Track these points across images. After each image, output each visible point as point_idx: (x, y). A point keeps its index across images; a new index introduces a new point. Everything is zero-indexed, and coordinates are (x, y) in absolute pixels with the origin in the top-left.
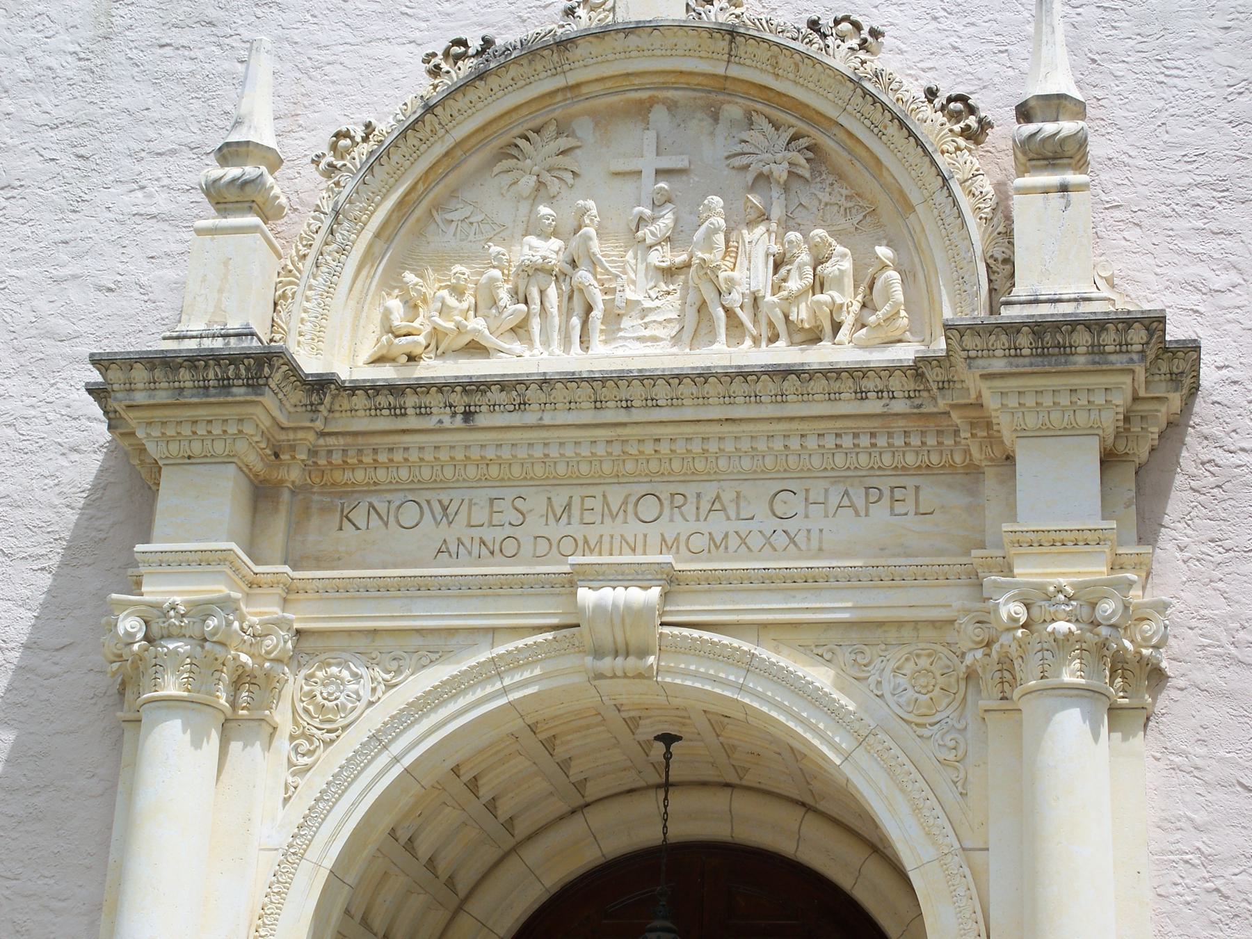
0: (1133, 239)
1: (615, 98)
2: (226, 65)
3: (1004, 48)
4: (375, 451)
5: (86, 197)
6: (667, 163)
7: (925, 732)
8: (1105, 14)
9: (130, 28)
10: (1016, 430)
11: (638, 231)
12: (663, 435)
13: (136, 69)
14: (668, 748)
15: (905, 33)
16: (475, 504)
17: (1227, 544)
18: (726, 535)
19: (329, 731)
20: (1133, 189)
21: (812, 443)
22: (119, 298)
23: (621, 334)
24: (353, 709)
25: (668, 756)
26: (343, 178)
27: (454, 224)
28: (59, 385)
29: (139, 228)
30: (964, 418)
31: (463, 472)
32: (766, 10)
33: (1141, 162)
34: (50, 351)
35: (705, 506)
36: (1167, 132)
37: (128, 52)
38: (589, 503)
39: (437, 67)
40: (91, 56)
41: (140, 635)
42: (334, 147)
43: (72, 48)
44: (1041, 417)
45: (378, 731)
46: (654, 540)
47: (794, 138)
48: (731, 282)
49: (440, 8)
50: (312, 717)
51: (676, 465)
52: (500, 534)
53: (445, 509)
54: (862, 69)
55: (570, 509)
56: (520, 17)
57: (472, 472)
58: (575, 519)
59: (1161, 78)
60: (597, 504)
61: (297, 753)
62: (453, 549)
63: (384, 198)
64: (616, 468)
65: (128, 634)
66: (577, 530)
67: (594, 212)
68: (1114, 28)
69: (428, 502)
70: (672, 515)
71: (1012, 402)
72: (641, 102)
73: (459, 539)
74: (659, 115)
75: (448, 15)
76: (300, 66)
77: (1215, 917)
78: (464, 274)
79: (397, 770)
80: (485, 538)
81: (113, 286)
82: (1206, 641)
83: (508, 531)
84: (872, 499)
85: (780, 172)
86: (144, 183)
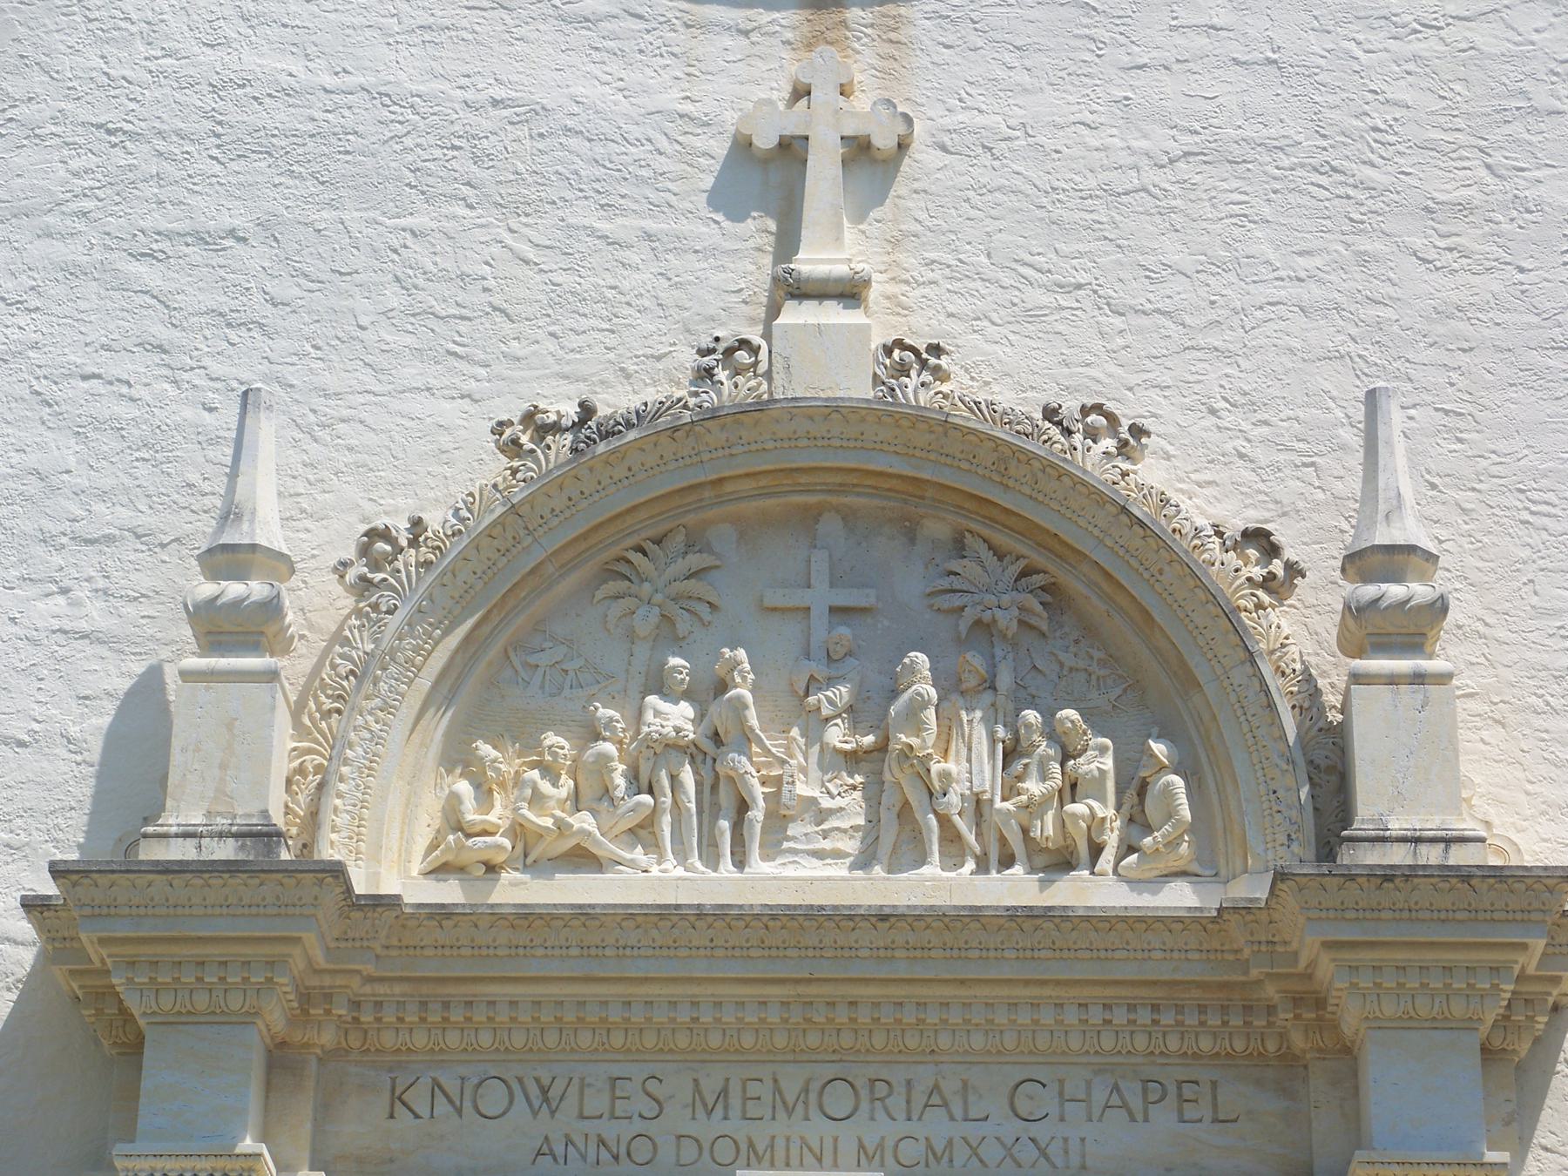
0: (1492, 741)
2: (188, 413)
3: (1310, 460)
4: (446, 1005)
6: (843, 598)
8: (1446, 420)
9: (35, 346)
10: (1367, 1018)
11: (807, 694)
12: (862, 997)
13: (47, 410)
15: (1173, 430)
16: (589, 1085)
18: (950, 1143)
20: (1491, 671)
21: (1071, 1017)
22: (36, 757)
23: (786, 845)
26: (384, 600)
27: (540, 672)
29: (62, 651)
30: (1285, 992)
31: (572, 1038)
32: (975, 384)
33: (1502, 634)
35: (919, 1099)
36: (1536, 593)
37: (34, 382)
38: (754, 1089)
39: (515, 442)
42: (364, 551)
44: (1402, 1003)
46: (848, 1149)
47: (1025, 573)
48: (946, 776)
49: (504, 348)
51: (879, 1040)
52: (627, 1130)
53: (544, 1091)
54: (1122, 483)
55: (726, 1097)
56: (622, 370)
57: (585, 1040)
58: (735, 1112)
59: (1526, 516)
60: (764, 1090)
62: (559, 1149)
63: (446, 633)
64: (793, 1042)
66: (738, 1128)
67: (747, 666)
68: (1460, 441)
69: (520, 1080)
70: (872, 1110)
71: (1365, 982)
72: (806, 508)
73: (567, 1136)
74: (831, 526)
75: (518, 359)
76: (299, 421)
78: (563, 748)
80: (604, 1135)
81: (27, 738)
83: (638, 1126)
84: (1152, 1098)
85: (1006, 620)
86: (66, 583)
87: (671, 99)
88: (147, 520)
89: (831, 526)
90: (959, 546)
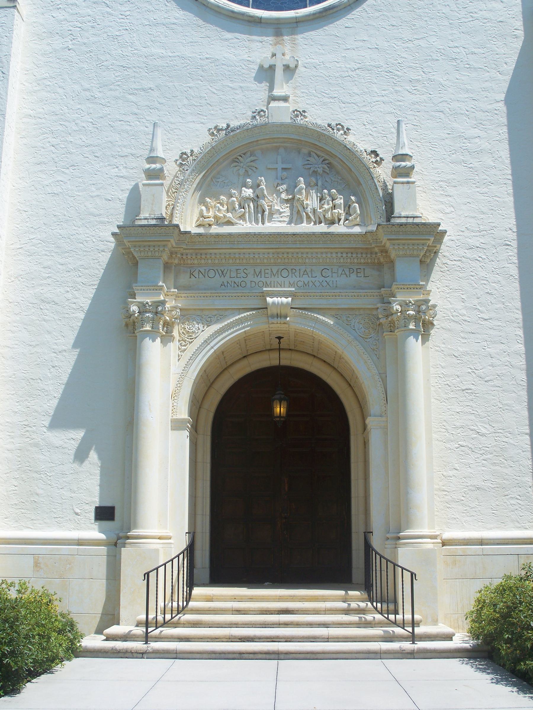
1: (268, 145)
2: (142, 128)
4: (201, 254)
5: (99, 170)
6: (285, 166)
7: (368, 340)
8: (414, 127)
9: (109, 114)
14: (280, 341)
17: (451, 287)
19: (190, 339)
21: (334, 255)
23: (273, 219)
24: (198, 332)
25: (279, 343)
28: (96, 230)
33: (425, 173)
34: (92, 219)
35: (302, 273)
40: (97, 123)
41: (137, 312)
43: (91, 120)
45: (206, 339)
46: (287, 284)
48: (307, 204)
50: (185, 335)
52: (240, 280)
53: (222, 272)
57: (231, 261)
60: (269, 271)
61: (181, 346)
62: (226, 284)
65: (133, 311)
66: (264, 280)
67: (264, 181)
68: (417, 131)
70: (292, 275)
74: (282, 150)
77: (447, 391)
79: (213, 350)
82: (445, 315)
83: (242, 279)
85: (320, 171)
86: (118, 166)
87: (245, 57)
88: (134, 152)
89: (282, 150)
90: (309, 155)
